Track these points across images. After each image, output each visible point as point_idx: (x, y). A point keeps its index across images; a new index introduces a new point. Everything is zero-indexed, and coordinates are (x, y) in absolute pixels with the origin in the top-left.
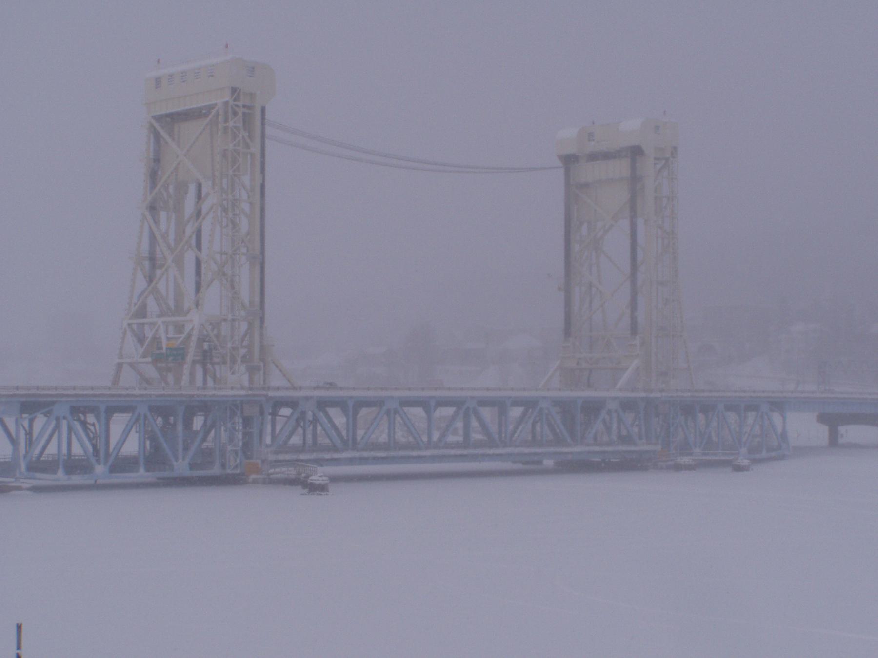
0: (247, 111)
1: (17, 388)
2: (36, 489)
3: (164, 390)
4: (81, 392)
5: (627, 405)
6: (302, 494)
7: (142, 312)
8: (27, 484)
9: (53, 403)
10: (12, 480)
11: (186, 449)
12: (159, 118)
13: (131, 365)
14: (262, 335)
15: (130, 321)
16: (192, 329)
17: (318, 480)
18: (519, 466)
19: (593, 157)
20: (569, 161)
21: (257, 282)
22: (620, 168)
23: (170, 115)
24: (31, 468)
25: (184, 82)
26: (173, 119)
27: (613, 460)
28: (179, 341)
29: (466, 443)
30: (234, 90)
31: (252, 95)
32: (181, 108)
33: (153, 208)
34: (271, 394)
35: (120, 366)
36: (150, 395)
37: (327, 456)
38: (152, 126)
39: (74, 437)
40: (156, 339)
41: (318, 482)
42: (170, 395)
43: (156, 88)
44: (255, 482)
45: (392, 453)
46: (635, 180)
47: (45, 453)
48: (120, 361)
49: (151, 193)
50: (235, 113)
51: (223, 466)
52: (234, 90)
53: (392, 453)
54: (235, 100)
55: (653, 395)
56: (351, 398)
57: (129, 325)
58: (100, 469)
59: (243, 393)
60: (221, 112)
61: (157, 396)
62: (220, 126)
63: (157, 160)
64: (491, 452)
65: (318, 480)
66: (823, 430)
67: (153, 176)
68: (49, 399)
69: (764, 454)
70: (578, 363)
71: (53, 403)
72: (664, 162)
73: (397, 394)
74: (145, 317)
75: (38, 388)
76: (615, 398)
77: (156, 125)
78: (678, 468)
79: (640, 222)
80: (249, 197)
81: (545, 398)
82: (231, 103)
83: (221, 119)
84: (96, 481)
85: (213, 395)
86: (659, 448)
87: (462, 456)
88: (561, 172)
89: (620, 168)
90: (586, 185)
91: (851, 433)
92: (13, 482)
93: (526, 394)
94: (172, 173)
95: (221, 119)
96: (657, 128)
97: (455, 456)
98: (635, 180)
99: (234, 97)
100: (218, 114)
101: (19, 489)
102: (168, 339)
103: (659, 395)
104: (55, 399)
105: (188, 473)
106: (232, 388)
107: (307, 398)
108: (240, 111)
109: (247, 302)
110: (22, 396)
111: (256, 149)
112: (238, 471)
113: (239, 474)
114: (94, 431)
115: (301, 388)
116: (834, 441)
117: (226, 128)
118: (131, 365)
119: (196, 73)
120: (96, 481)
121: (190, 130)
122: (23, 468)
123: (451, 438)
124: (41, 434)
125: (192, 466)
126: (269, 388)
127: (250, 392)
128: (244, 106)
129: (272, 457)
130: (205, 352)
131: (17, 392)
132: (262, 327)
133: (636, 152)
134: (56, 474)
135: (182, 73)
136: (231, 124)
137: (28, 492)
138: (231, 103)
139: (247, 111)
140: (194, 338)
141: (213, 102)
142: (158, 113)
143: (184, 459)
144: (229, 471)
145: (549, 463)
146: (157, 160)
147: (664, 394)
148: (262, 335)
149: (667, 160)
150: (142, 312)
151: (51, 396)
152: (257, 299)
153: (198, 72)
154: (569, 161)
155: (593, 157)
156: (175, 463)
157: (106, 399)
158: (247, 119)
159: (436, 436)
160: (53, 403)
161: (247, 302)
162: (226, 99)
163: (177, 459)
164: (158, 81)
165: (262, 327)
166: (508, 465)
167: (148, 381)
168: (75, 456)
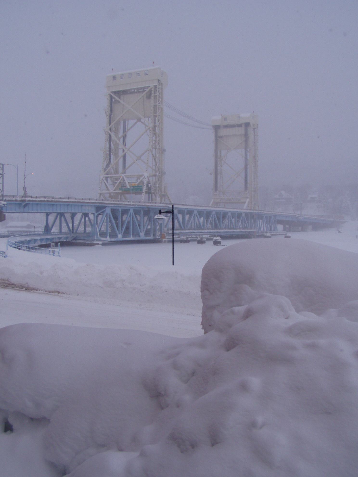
2: (104, 244)
3: (140, 203)
9: (105, 207)
17: (219, 240)
19: (226, 126)
20: (217, 128)
22: (241, 131)
25: (130, 77)
26: (119, 93)
28: (137, 183)
32: (121, 89)
36: (135, 205)
43: (113, 80)
44: (165, 242)
47: (52, 230)
51: (154, 235)
71: (105, 207)
89: (241, 131)
98: (246, 135)
101: (98, 244)
104: (106, 205)
119: (137, 74)
133: (247, 125)
134: (130, 237)
135: (129, 74)
143: (143, 233)
153: (139, 73)
154: (217, 128)
155: (226, 126)
156: (141, 234)
157: (113, 205)
160: (106, 206)
163: (141, 233)
164: (114, 78)
168: (63, 233)
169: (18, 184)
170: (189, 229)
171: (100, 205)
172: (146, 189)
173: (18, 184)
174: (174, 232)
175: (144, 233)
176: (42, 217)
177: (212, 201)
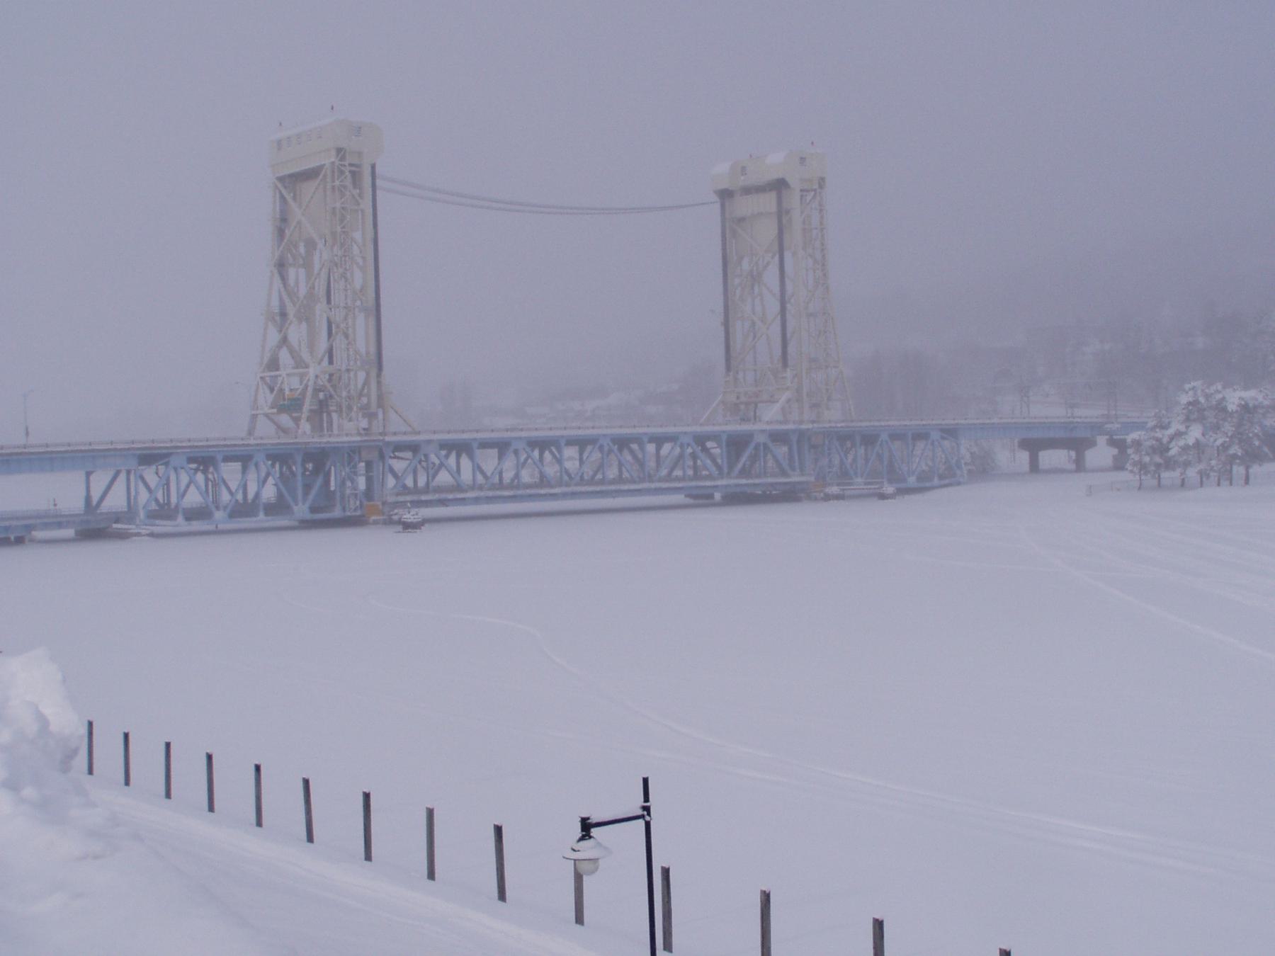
0: (353, 169)
1: (133, 442)
2: (152, 535)
4: (196, 444)
5: (779, 437)
6: (396, 532)
7: (273, 364)
8: (145, 530)
10: (134, 527)
11: (306, 494)
12: (281, 179)
13: (267, 415)
14: (379, 383)
15: (262, 375)
16: (309, 380)
17: (410, 518)
18: (690, 501)
19: (747, 191)
20: (725, 195)
21: (372, 332)
23: (291, 176)
24: (153, 516)
27: (774, 492)
29: (543, 481)
30: (339, 150)
31: (360, 154)
33: (281, 266)
34: (387, 439)
35: (254, 417)
36: (265, 444)
37: (451, 496)
38: (276, 187)
39: (183, 488)
40: (281, 390)
41: (409, 520)
42: (284, 444)
44: (376, 523)
45: (520, 492)
46: (782, 214)
48: (254, 412)
49: (279, 246)
50: (342, 172)
51: (344, 509)
52: (339, 150)
53: (520, 492)
54: (341, 160)
55: (804, 427)
56: (646, 434)
57: (261, 378)
58: (219, 515)
59: (358, 438)
60: (329, 173)
61: (272, 444)
62: (329, 186)
63: (284, 220)
64: (543, 491)
65: (410, 518)
66: (1024, 456)
67: (281, 233)
68: (164, 451)
69: (936, 481)
70: (738, 398)
72: (813, 193)
73: (524, 434)
74: (277, 369)
75: (153, 441)
76: (763, 431)
77: (279, 185)
78: (828, 498)
79: (788, 256)
80: (361, 252)
81: (685, 433)
82: (337, 163)
83: (329, 179)
84: (217, 527)
85: (328, 442)
86: (812, 479)
87: (597, 492)
88: (717, 207)
89: (768, 202)
90: (742, 220)
91: (1050, 458)
92: (134, 529)
93: (580, 432)
94: (295, 227)
95: (329, 179)
96: (803, 160)
97: (592, 493)
98: (782, 214)
99: (340, 156)
100: (325, 176)
101: (138, 534)
102: (291, 390)
103: (810, 426)
105: (309, 516)
106: (347, 435)
107: (429, 442)
108: (347, 170)
109: (363, 351)
110: (139, 449)
111: (366, 204)
112: (358, 513)
113: (360, 516)
114: (212, 479)
115: (419, 433)
116: (1034, 467)
117: (333, 188)
118: (267, 415)
120: (217, 527)
121: (309, 188)
122: (142, 515)
123: (678, 473)
124: (136, 486)
125: (313, 510)
126: (385, 435)
127: (366, 438)
128: (351, 165)
129: (391, 499)
130: (321, 402)
131: (133, 446)
132: (379, 375)
133: (779, 185)
136: (337, 183)
137: (147, 538)
138: (337, 163)
139: (353, 169)
140: (310, 390)
141: (323, 163)
142: (282, 174)
143: (303, 504)
144: (348, 514)
145: (718, 496)
146: (284, 220)
147: (815, 425)
148: (379, 383)
149: (815, 190)
150: (273, 364)
151: (167, 448)
152: (373, 349)
154: (725, 195)
155: (747, 191)
158: (356, 176)
159: (664, 472)
160: (171, 454)
161: (363, 351)
162: (333, 160)
164: (279, 142)
165: (379, 375)
166: (679, 498)
167: (285, 431)
169: (682, 207)
170: (576, 485)
171: (148, 452)
172: (310, 405)
173: (682, 207)
174: (1161, 476)
175: (307, 504)
176: (79, 476)
177: (720, 398)
